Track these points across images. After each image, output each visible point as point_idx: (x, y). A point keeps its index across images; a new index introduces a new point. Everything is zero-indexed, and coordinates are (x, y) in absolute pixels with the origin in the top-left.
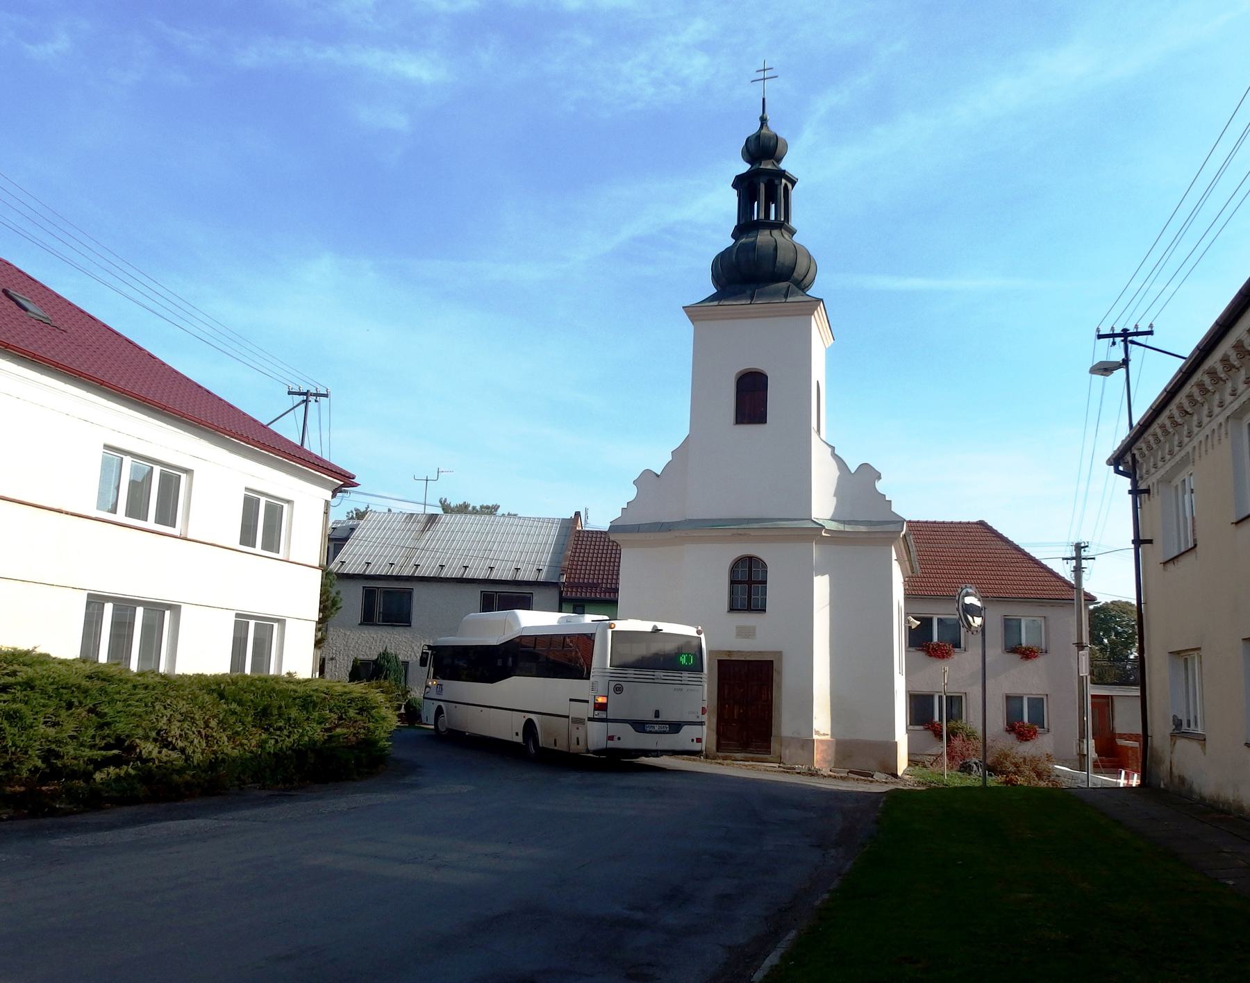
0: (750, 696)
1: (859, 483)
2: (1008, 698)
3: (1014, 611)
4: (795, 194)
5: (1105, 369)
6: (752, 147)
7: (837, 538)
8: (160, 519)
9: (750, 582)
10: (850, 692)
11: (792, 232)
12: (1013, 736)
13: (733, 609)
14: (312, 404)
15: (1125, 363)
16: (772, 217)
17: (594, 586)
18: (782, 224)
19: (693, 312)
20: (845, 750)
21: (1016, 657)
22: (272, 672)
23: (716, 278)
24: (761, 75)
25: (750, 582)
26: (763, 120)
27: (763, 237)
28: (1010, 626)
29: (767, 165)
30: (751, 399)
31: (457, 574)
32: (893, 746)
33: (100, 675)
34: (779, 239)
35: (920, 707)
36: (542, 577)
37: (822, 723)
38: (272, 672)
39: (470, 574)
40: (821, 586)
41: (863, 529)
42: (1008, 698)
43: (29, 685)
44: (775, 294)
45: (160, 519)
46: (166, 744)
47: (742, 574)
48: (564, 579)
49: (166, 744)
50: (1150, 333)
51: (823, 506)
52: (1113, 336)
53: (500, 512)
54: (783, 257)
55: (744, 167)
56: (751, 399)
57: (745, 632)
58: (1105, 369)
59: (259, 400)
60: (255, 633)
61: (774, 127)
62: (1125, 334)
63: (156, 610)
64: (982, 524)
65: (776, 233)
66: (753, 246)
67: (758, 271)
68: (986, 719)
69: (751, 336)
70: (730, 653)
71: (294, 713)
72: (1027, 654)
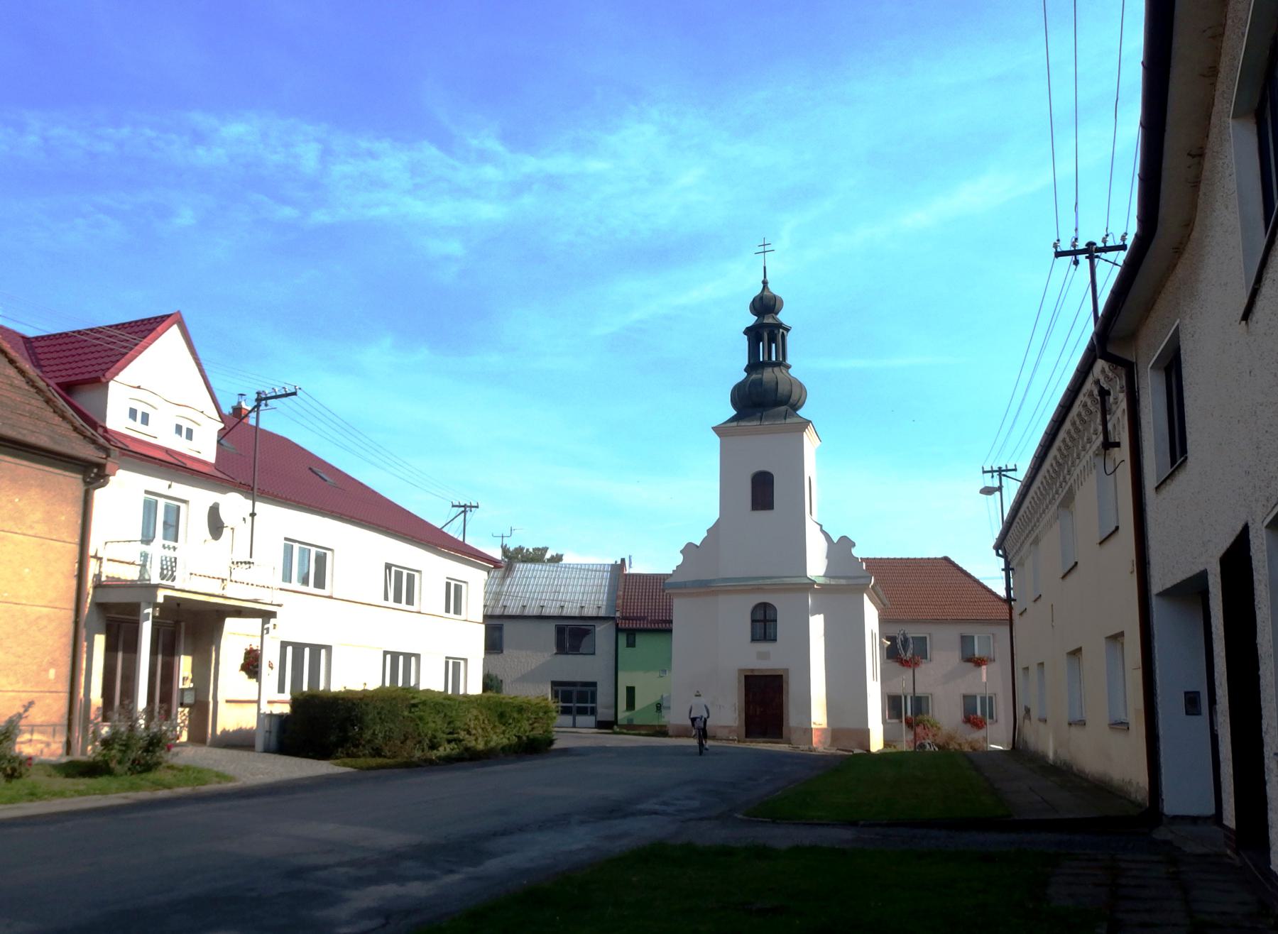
0: (767, 699)
1: (840, 549)
2: (965, 697)
3: (967, 630)
4: (790, 338)
5: (987, 491)
6: (757, 305)
7: (825, 589)
8: (456, 613)
9: (765, 621)
10: (845, 693)
11: (788, 367)
12: (969, 726)
13: (754, 640)
14: (468, 514)
15: (1000, 489)
16: (774, 359)
17: (643, 618)
18: (782, 364)
19: (718, 430)
20: (835, 733)
21: (970, 665)
22: (461, 692)
23: (735, 403)
24: (761, 249)
25: (765, 621)
26: (765, 283)
27: (768, 374)
28: (966, 641)
29: (768, 320)
30: (762, 491)
31: (535, 612)
32: (866, 733)
33: (448, 698)
34: (780, 375)
35: (893, 704)
36: (602, 613)
37: (819, 717)
38: (321, 688)
39: (546, 612)
40: (817, 624)
41: (843, 582)
42: (965, 697)
43: (424, 703)
44: (776, 417)
45: (456, 613)
46: (469, 733)
47: (760, 616)
48: (618, 614)
49: (469, 733)
50: (1015, 470)
51: (816, 566)
52: (992, 471)
53: (548, 556)
54: (783, 389)
55: (751, 320)
56: (762, 491)
57: (763, 656)
58: (987, 491)
59: (435, 514)
60: (455, 667)
61: (774, 289)
62: (1000, 470)
63: (316, 649)
64: (946, 559)
65: (776, 369)
66: (760, 382)
67: (765, 399)
68: (946, 716)
69: (761, 448)
70: (752, 670)
71: (515, 715)
72: (979, 662)
